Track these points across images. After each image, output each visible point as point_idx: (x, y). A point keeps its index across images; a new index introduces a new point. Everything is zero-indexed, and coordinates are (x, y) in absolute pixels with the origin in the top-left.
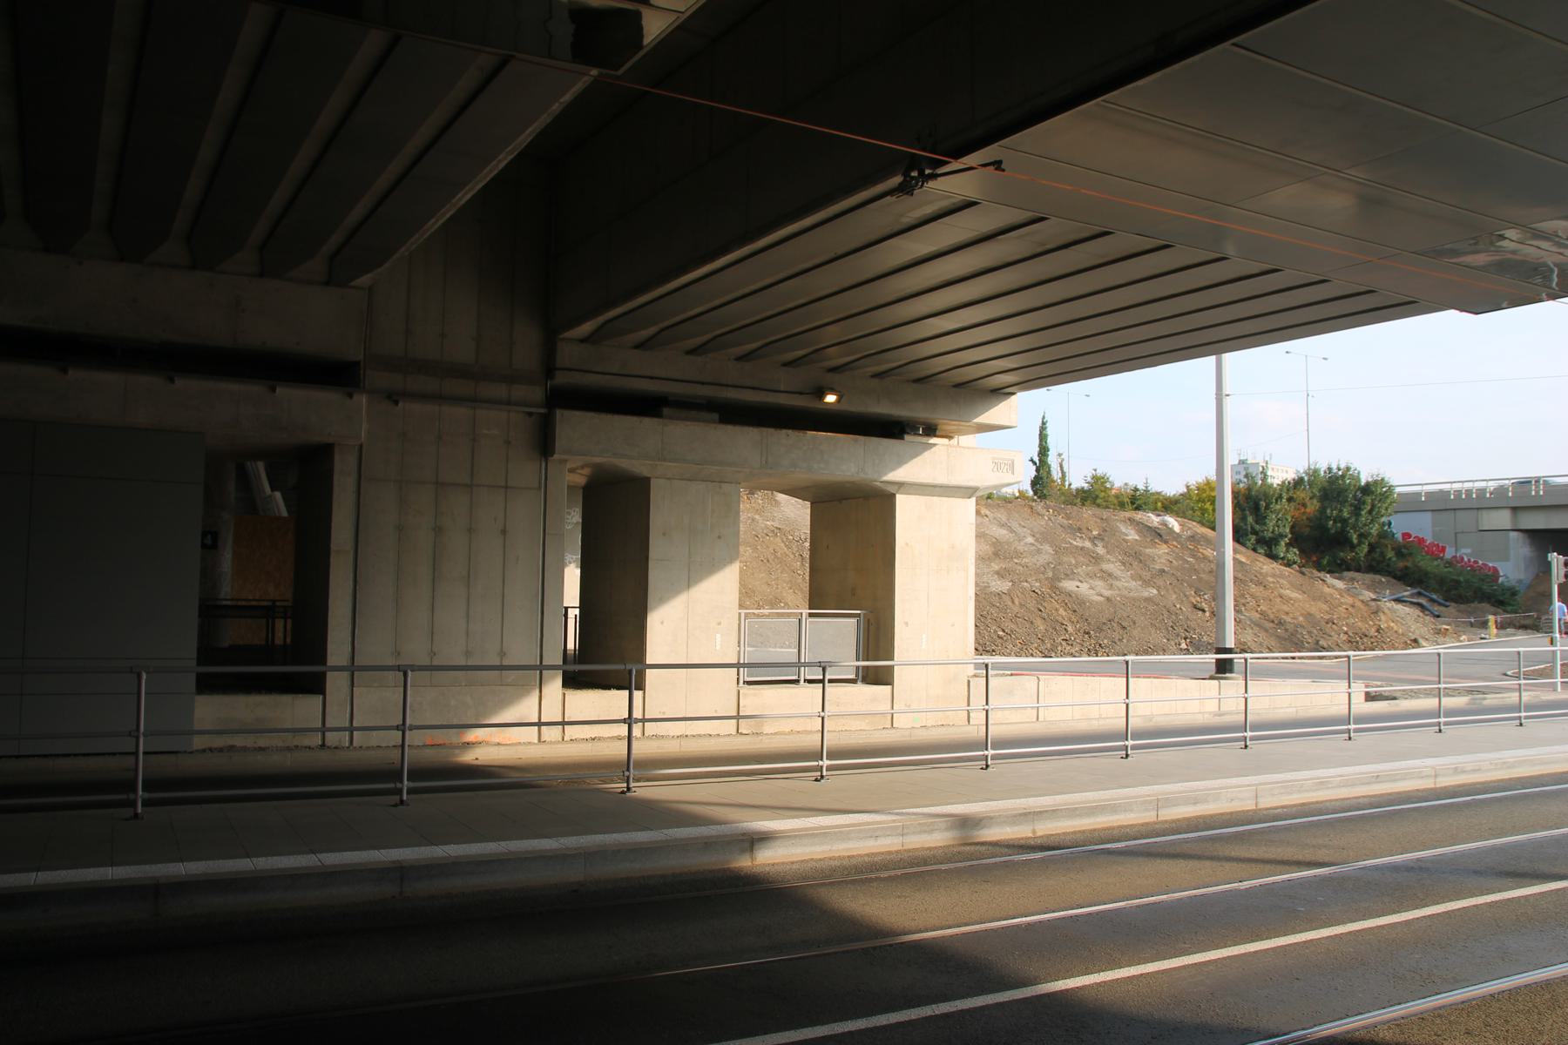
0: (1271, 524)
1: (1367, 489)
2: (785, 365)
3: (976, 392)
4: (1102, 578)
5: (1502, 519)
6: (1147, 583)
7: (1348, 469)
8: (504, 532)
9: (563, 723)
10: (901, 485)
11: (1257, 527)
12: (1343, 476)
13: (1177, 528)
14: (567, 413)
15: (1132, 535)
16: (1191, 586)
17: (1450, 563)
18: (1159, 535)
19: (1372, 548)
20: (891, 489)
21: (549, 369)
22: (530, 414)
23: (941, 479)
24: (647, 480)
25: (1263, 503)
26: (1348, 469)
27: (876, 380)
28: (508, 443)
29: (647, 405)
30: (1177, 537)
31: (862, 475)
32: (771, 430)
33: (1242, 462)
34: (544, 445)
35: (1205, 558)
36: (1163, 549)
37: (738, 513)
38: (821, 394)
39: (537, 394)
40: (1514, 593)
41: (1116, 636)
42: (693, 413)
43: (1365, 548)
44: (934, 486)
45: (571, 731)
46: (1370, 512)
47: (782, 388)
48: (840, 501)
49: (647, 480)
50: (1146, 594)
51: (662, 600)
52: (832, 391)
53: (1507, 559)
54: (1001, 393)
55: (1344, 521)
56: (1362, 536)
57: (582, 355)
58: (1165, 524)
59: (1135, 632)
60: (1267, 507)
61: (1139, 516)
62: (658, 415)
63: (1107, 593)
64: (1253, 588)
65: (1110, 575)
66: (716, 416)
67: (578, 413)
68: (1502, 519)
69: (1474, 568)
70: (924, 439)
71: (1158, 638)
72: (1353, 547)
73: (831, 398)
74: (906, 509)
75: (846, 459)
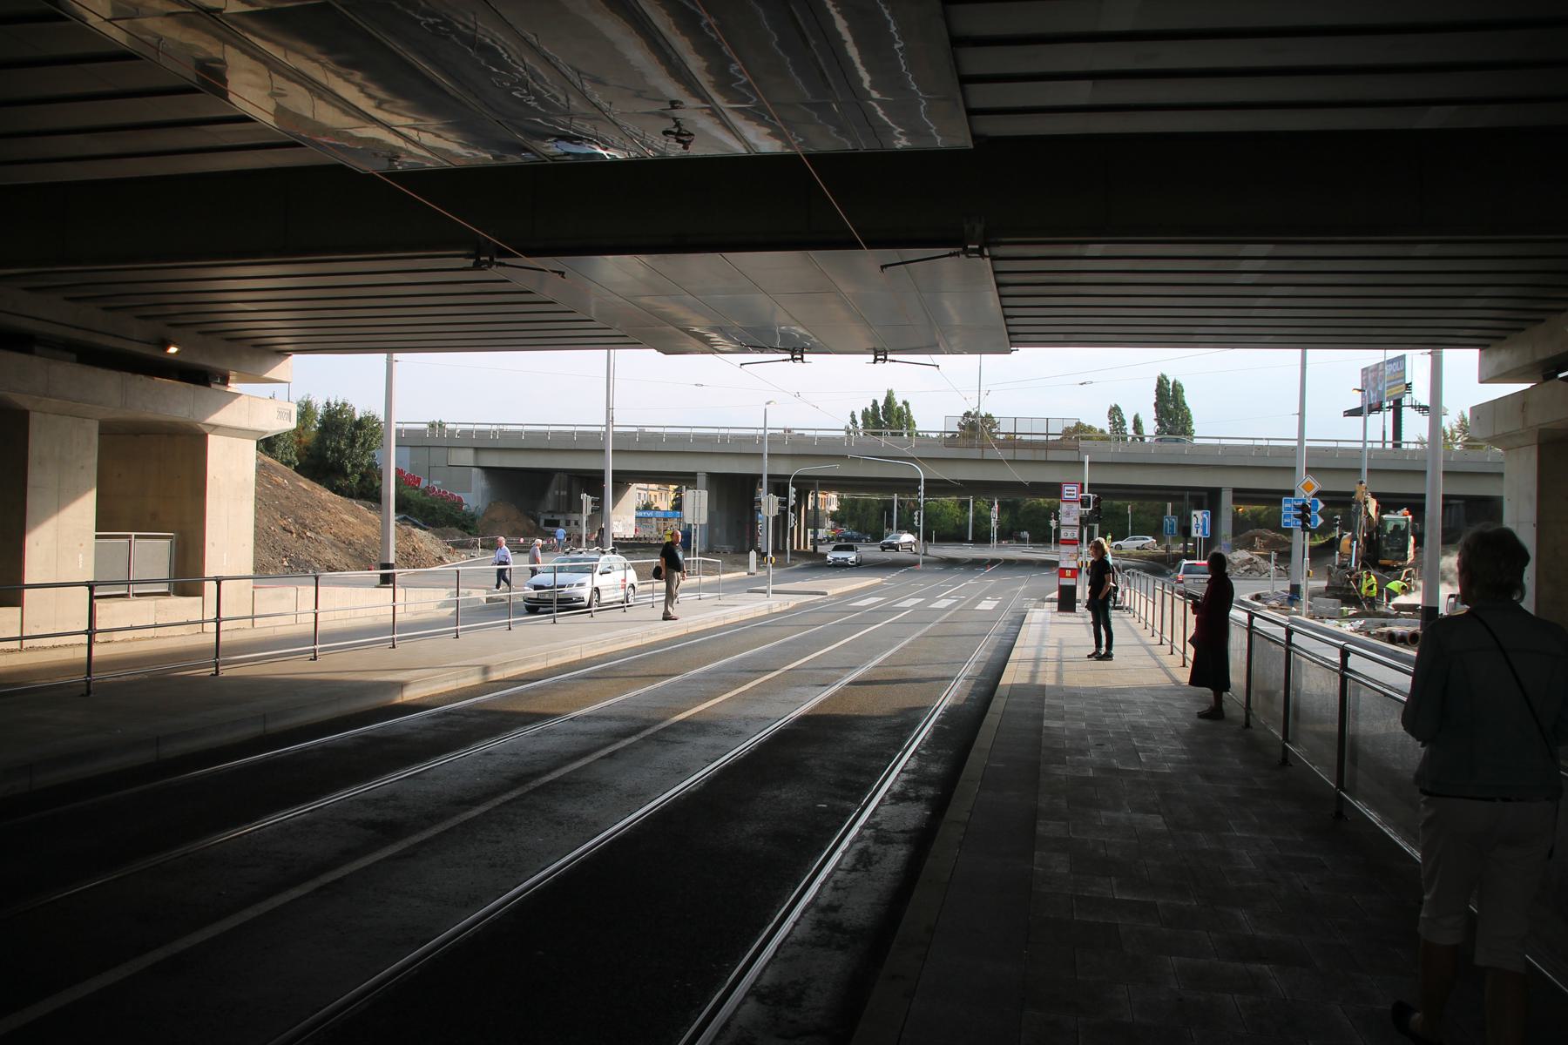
1: (359, 425)
3: (261, 351)
5: (467, 457)
7: (345, 405)
9: (22, 638)
12: (340, 411)
16: (276, 509)
17: (425, 493)
19: (363, 477)
20: (206, 430)
23: (244, 424)
26: (345, 405)
35: (279, 485)
40: (473, 518)
43: (357, 477)
45: (27, 643)
46: (363, 444)
51: (37, 524)
52: (175, 345)
53: (469, 491)
54: (283, 354)
55: (338, 450)
56: (354, 466)
62: (30, 352)
64: (324, 514)
66: (74, 356)
68: (467, 457)
69: (443, 497)
70: (223, 388)
72: (346, 476)
73: (173, 350)
74: (215, 444)
75: (170, 402)
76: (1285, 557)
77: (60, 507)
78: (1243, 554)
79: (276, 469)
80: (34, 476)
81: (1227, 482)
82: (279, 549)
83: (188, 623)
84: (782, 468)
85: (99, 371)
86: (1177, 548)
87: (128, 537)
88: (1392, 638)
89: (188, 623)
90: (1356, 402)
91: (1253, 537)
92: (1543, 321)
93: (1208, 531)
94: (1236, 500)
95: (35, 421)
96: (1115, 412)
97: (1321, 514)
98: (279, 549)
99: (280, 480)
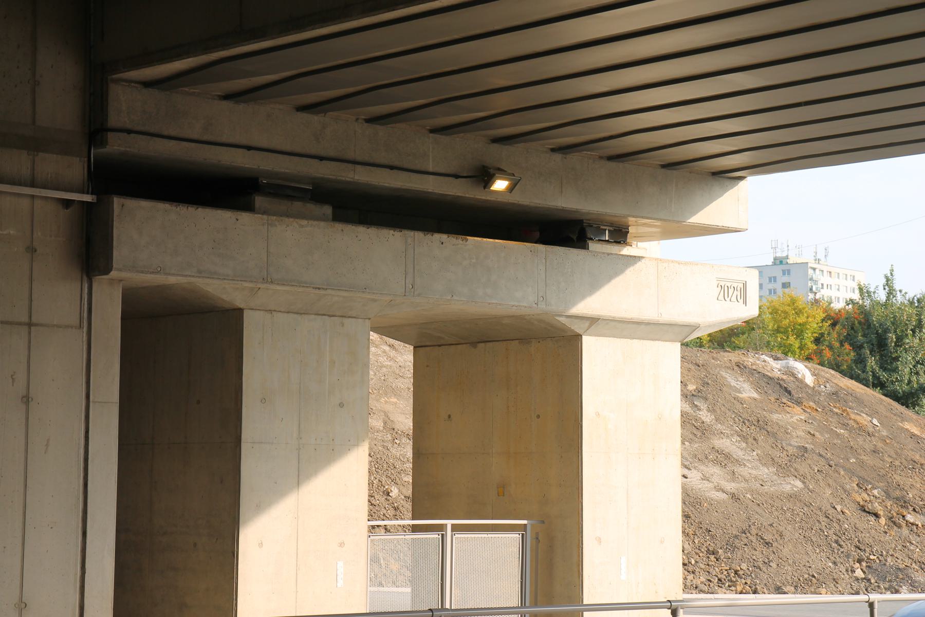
0: (905, 370)
2: (611, 158)
3: (687, 172)
4: (716, 462)
6: (785, 470)
8: (26, 399)
10: (593, 321)
11: (883, 376)
13: (809, 380)
14: (132, 204)
15: (748, 392)
16: (851, 473)
18: (785, 390)
20: (577, 327)
21: (95, 129)
22: (67, 203)
23: (649, 313)
24: (238, 313)
25: (892, 336)
27: (558, 157)
28: (31, 250)
29: (228, 191)
30: (813, 393)
31: (542, 306)
32: (419, 235)
33: (779, 261)
34: (91, 252)
35: (861, 428)
36: (796, 415)
37: (366, 365)
38: (485, 176)
39: (74, 168)
41: (759, 556)
42: (298, 205)
44: (639, 323)
47: (431, 169)
48: (474, 344)
49: (238, 313)
50: (787, 488)
51: (260, 508)
52: (502, 172)
54: (726, 176)
57: (151, 115)
58: (791, 373)
59: (786, 551)
60: (899, 341)
61: (750, 359)
62: (249, 208)
63: (730, 486)
65: (728, 456)
66: (328, 210)
67: (145, 204)
70: (614, 249)
71: (819, 561)
73: (500, 185)
74: (597, 356)
75: (505, 280)
77: (300, 477)
79: (859, 401)
80: (263, 426)
82: (848, 547)
84: (838, 270)
85: (362, 231)
87: (441, 528)
95: (252, 324)
98: (848, 547)
99: (864, 419)
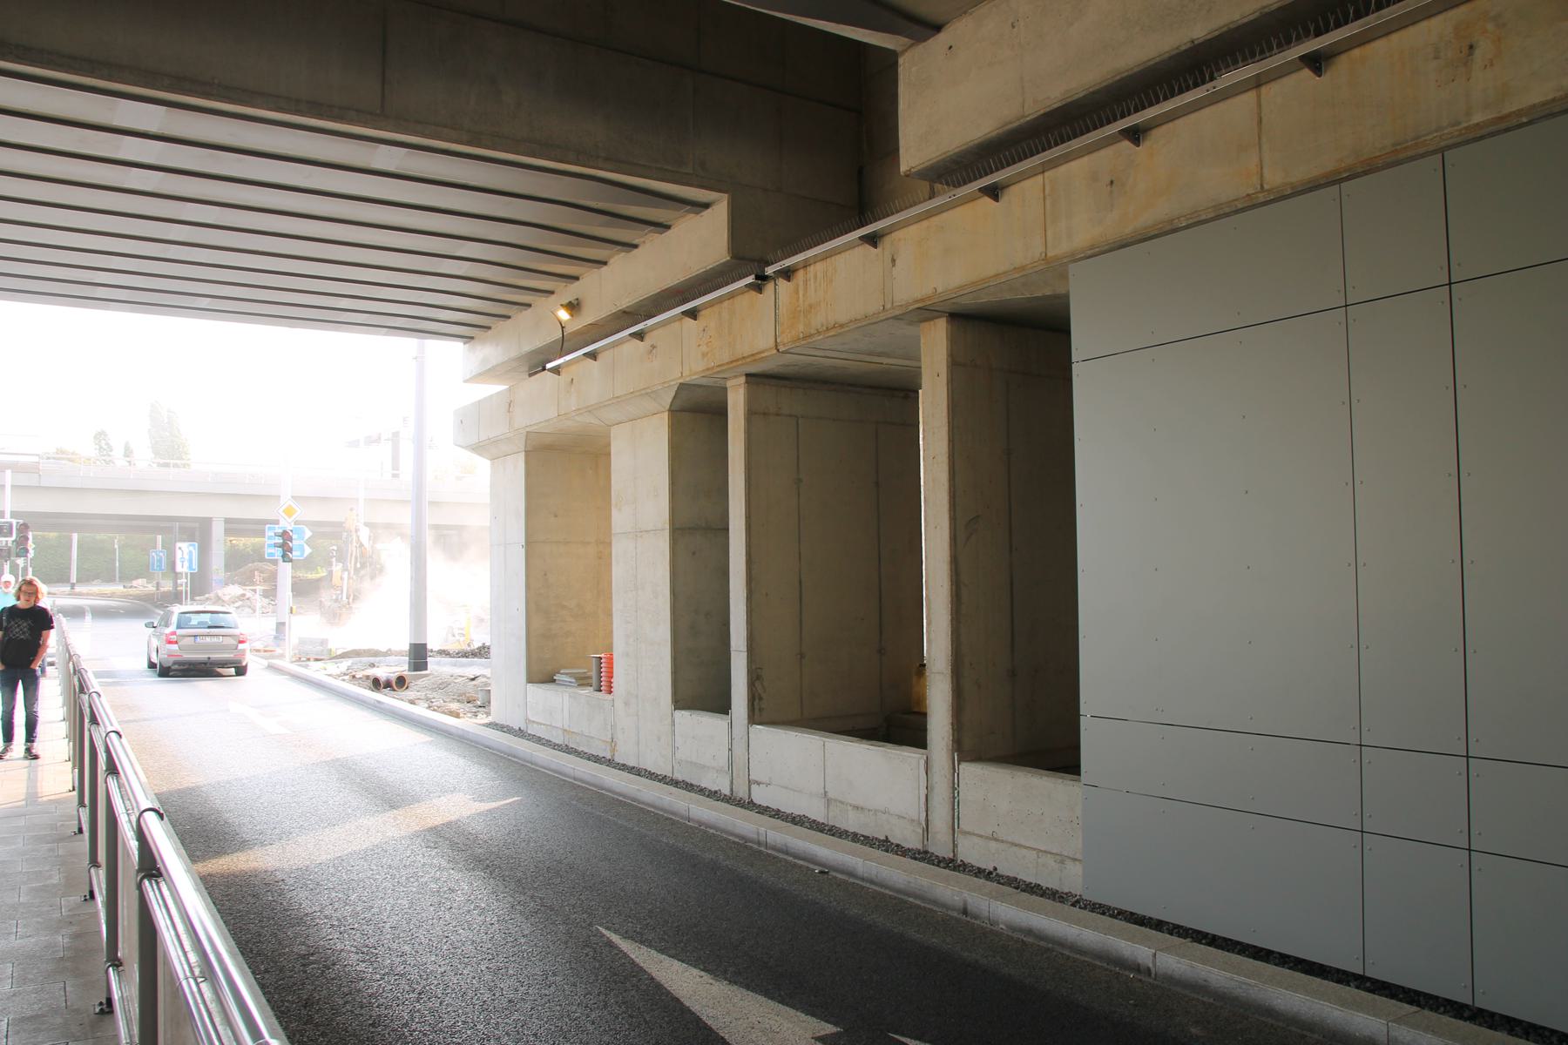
75: (22, 604)
76: (271, 594)
78: (235, 590)
81: (219, 512)
83: (689, 787)
86: (167, 586)
88: (376, 684)
89: (689, 787)
90: (830, 795)
91: (252, 572)
92: (664, 227)
93: (195, 566)
94: (228, 532)
96: (100, 436)
97: (308, 542)
